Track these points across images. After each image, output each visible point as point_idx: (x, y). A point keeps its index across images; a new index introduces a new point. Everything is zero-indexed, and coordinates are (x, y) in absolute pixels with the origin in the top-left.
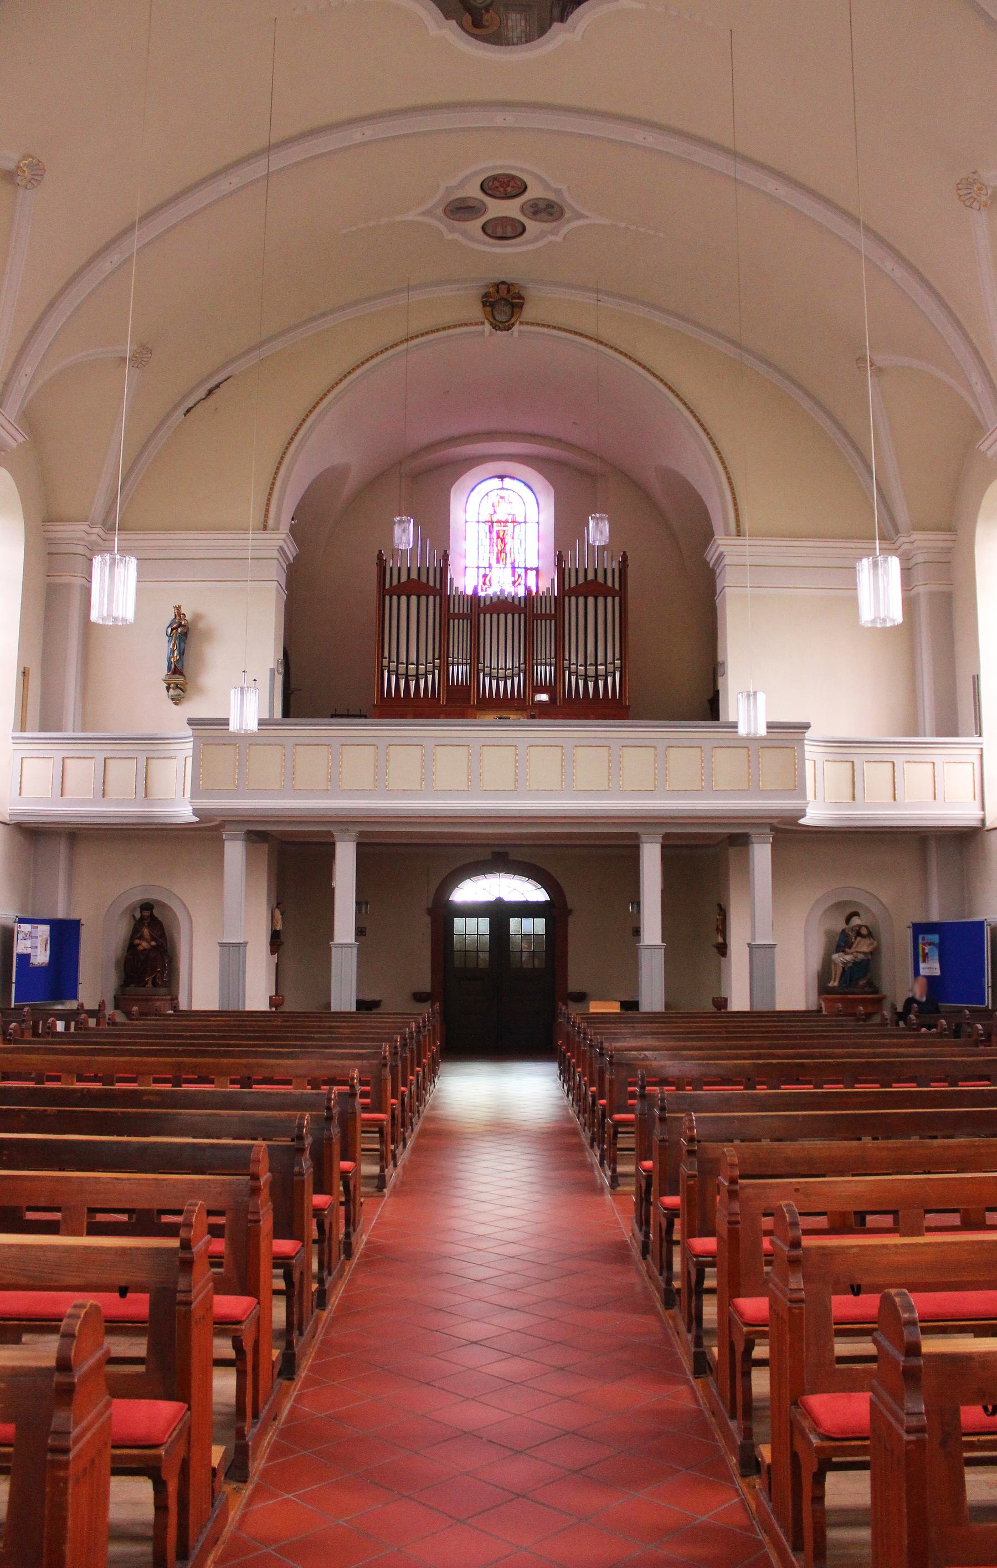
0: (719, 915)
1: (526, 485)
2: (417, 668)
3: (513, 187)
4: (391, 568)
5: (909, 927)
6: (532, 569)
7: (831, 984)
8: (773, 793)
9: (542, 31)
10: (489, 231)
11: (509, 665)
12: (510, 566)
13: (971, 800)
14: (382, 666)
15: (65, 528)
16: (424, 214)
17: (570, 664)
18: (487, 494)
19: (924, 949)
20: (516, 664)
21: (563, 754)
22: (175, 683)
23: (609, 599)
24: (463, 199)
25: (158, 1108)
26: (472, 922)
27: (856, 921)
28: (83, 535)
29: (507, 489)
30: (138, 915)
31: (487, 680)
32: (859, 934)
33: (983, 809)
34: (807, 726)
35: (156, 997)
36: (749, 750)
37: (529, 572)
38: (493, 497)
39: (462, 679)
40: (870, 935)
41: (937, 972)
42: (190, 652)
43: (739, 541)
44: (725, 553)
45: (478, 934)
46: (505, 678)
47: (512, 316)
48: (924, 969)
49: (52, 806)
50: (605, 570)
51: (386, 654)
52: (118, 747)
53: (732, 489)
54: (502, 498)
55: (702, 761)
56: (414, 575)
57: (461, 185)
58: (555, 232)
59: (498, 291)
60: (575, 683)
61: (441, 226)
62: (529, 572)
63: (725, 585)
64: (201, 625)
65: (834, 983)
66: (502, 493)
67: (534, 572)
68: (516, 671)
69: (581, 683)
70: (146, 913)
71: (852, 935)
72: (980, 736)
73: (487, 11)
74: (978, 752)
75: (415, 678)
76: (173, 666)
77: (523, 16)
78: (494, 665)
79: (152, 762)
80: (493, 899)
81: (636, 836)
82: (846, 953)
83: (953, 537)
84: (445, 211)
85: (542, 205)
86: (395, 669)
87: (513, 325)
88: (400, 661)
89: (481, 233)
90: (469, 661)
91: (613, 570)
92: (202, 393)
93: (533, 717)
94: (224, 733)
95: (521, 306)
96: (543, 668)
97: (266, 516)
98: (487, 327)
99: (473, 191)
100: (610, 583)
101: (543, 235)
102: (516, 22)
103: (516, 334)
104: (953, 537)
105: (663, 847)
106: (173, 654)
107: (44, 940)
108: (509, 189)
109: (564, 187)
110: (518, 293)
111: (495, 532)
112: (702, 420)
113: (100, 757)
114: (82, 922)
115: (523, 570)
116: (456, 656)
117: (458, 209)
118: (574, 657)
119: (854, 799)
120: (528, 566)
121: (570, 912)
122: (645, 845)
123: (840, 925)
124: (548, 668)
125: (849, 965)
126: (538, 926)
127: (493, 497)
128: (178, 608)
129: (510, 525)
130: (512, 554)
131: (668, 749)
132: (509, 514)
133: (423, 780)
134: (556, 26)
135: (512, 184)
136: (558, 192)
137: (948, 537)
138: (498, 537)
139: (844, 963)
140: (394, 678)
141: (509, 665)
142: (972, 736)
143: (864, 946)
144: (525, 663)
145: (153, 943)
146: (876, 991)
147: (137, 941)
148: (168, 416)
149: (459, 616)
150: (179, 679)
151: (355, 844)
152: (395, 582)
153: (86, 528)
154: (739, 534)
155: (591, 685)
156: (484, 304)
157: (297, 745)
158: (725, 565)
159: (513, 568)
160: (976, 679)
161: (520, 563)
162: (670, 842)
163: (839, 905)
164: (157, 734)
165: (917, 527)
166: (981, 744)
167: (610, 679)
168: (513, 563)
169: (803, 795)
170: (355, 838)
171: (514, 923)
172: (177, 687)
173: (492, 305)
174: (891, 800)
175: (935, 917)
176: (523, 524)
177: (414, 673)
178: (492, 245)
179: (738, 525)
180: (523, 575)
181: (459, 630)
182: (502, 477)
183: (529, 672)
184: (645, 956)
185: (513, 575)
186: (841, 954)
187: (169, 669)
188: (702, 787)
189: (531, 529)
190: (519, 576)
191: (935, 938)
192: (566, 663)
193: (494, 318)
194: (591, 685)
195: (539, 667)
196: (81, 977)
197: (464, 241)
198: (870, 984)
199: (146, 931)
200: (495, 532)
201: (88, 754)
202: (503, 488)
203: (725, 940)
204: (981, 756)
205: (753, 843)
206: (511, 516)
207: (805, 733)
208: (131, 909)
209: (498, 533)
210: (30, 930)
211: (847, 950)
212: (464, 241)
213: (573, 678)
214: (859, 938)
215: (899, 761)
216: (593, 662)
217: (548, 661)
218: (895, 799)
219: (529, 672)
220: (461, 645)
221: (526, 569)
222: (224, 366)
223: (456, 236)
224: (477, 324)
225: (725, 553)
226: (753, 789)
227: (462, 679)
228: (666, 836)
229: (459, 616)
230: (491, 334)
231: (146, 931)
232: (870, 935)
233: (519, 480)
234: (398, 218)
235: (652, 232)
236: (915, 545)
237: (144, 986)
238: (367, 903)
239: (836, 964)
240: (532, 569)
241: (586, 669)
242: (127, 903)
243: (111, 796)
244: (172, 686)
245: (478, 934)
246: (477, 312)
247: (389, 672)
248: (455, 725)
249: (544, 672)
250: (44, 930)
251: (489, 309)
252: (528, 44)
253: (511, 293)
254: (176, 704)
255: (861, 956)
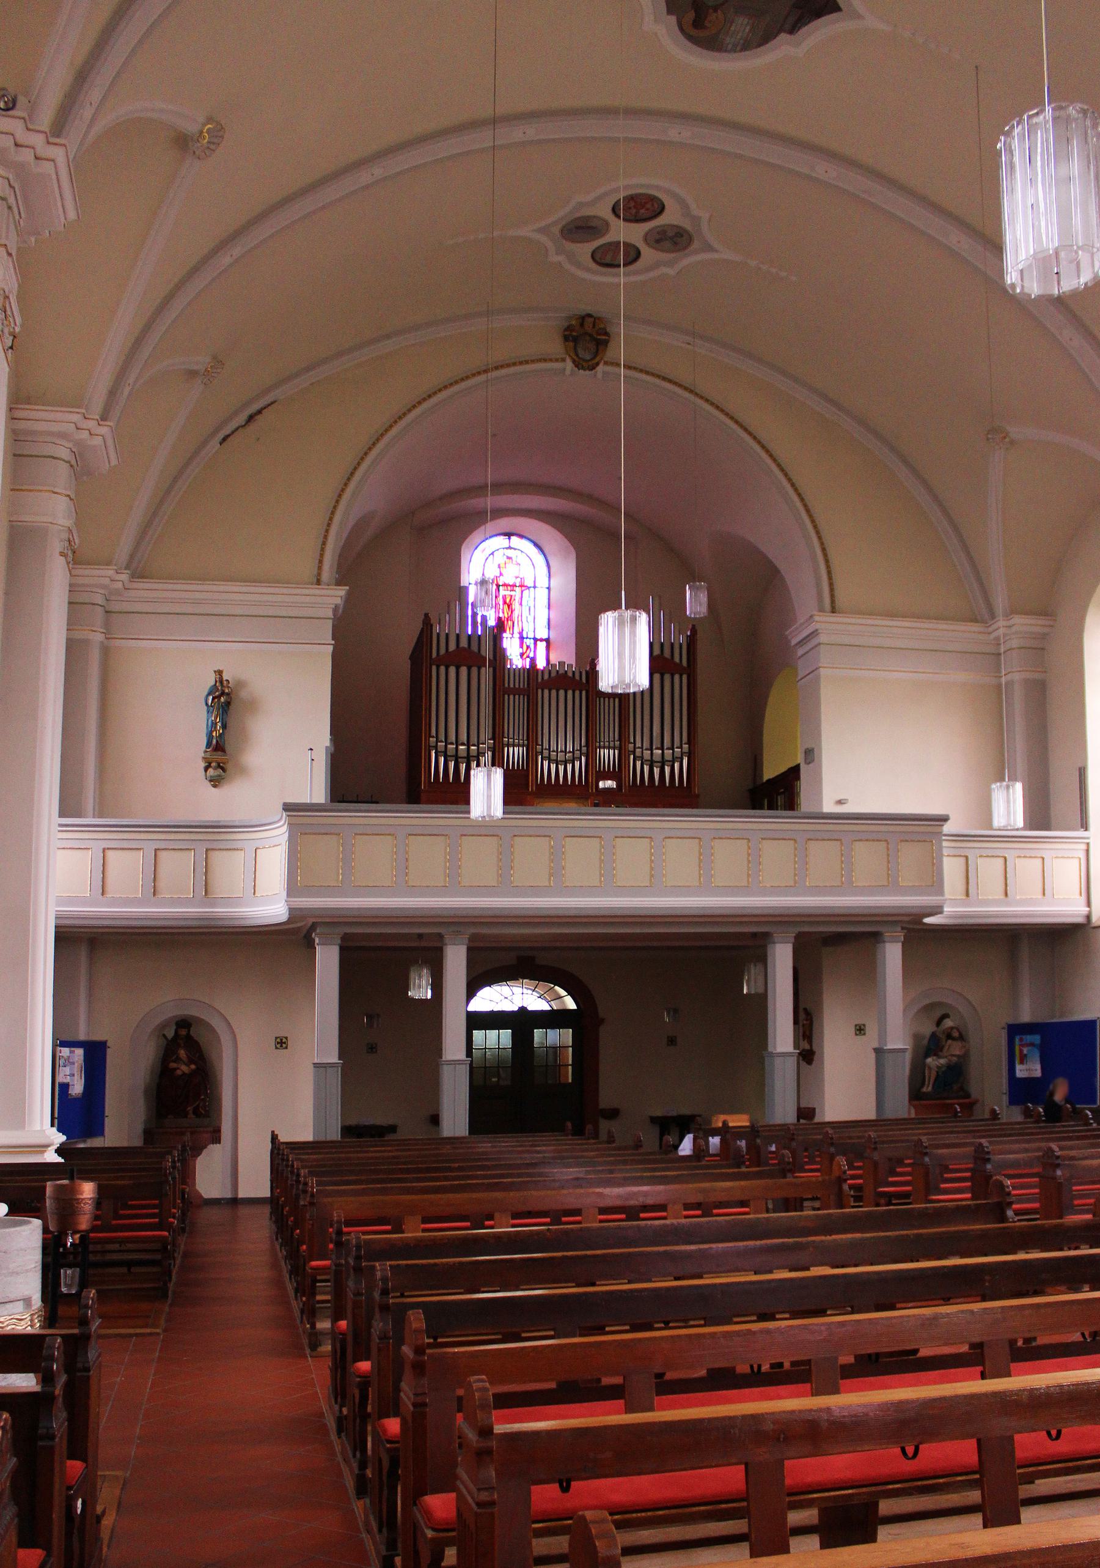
0: (807, 1020)
1: (536, 545)
2: (468, 749)
3: (647, 209)
4: (438, 635)
5: (1003, 1028)
6: (541, 640)
7: (924, 1090)
8: (776, 890)
9: (765, 39)
10: (597, 259)
11: (570, 748)
12: (518, 636)
13: (1078, 897)
14: (503, 744)
15: (87, 572)
16: (541, 230)
17: (635, 748)
18: (493, 553)
19: (1021, 1051)
20: (577, 747)
21: (700, 847)
22: (216, 762)
23: (677, 677)
24: (588, 218)
25: (625, 1247)
26: (492, 1034)
27: (948, 1023)
28: (107, 581)
29: (515, 549)
30: (170, 1033)
31: (546, 763)
32: (949, 1036)
33: (1089, 904)
34: (944, 819)
35: (202, 1129)
36: (842, 844)
37: (538, 642)
38: (499, 558)
39: (513, 763)
40: (961, 1038)
41: (1038, 1073)
42: (231, 723)
43: (833, 618)
44: (819, 631)
45: (499, 1048)
46: (565, 763)
47: (596, 354)
48: (1021, 1071)
49: (91, 906)
50: (672, 645)
51: (433, 733)
52: (172, 837)
53: (827, 561)
54: (509, 558)
55: (842, 855)
56: (464, 643)
57: (593, 203)
58: (670, 264)
59: (582, 325)
60: (639, 769)
61: (550, 245)
62: (538, 642)
63: (820, 665)
64: (244, 694)
65: (928, 1089)
66: (510, 553)
67: (544, 643)
68: (577, 753)
69: (646, 768)
70: (183, 1032)
71: (943, 1037)
72: (1086, 830)
73: (715, 11)
74: (1084, 847)
75: (475, 758)
76: (214, 741)
77: (751, 21)
78: (553, 747)
79: (211, 853)
80: (516, 1009)
81: (440, 936)
82: (939, 1057)
83: (1051, 623)
84: (562, 231)
85: (667, 244)
86: (640, 755)
87: (598, 364)
88: (449, 741)
89: (591, 260)
90: (617, 743)
91: (681, 645)
92: (242, 418)
93: (596, 805)
94: (466, 822)
95: (606, 343)
96: (606, 751)
97: (320, 568)
98: (569, 365)
99: (604, 211)
100: (677, 659)
101: (657, 265)
102: (741, 26)
103: (600, 375)
104: (1051, 623)
105: (469, 950)
106: (216, 727)
107: (80, 1066)
108: (642, 211)
109: (704, 215)
110: (605, 329)
111: (501, 597)
112: (797, 485)
113: (150, 848)
114: (108, 1044)
115: (532, 641)
116: (511, 736)
117: (578, 228)
118: (638, 740)
119: (967, 895)
120: (538, 637)
121: (602, 1021)
122: (449, 946)
123: (928, 1029)
124: (611, 752)
125: (943, 1069)
126: (561, 1037)
127: (499, 558)
128: (219, 673)
129: (518, 590)
130: (520, 623)
131: (854, 843)
132: (517, 577)
133: (551, 875)
134: (783, 36)
135: (649, 206)
136: (696, 220)
137: (1047, 623)
138: (505, 602)
139: (938, 1067)
140: (442, 760)
141: (570, 748)
142: (1078, 830)
143: (955, 1049)
144: (587, 745)
145: (193, 1067)
146: (968, 1096)
147: (173, 1065)
148: (204, 443)
149: (515, 692)
150: (219, 756)
151: (465, 947)
152: (443, 651)
153: (111, 573)
154: (833, 610)
155: (656, 771)
156: (566, 338)
157: (410, 835)
158: (820, 644)
159: (522, 638)
160: (1082, 773)
161: (528, 631)
162: (476, 944)
163: (928, 1008)
164: (219, 821)
165: (1013, 611)
166: (1088, 838)
167: (677, 765)
168: (521, 633)
169: (940, 891)
170: (467, 941)
171: (538, 1033)
172: (219, 766)
173: (575, 340)
174: (1002, 897)
175: (1026, 1017)
176: (532, 589)
177: (659, 759)
178: (604, 274)
179: (833, 601)
180: (532, 646)
181: (515, 706)
182: (509, 535)
183: (590, 756)
184: (446, 1072)
185: (521, 646)
186: (935, 1058)
187: (209, 744)
188: (795, 882)
189: (542, 595)
190: (528, 647)
191: (1036, 1039)
192: (631, 746)
193: (577, 355)
194: (656, 771)
195: (602, 751)
196: (108, 1111)
197: (567, 266)
198: (962, 1089)
199: (182, 1053)
200: (501, 597)
201: (134, 845)
202: (510, 548)
203: (811, 1046)
204: (1087, 851)
205: (774, 943)
206: (519, 580)
207: (943, 825)
208: (164, 1025)
209: (504, 597)
210: (68, 1054)
211: (940, 1053)
212: (567, 266)
213: (638, 764)
214: (950, 1042)
215: (971, 855)
216: (649, 747)
217: (612, 744)
218: (1006, 894)
219: (590, 756)
220: (516, 725)
221: (536, 640)
222: (269, 390)
223: (561, 258)
224: (557, 360)
225: (819, 631)
226: (892, 885)
227: (513, 763)
228: (345, 937)
229: (515, 692)
230: (572, 374)
231: (182, 1053)
232: (961, 1038)
233: (529, 539)
234: (512, 233)
235: (784, 274)
236: (1014, 629)
237: (186, 1117)
238: (378, 1015)
239: (930, 1068)
240: (541, 640)
241: (652, 754)
242: (158, 1021)
243: (165, 894)
244: (213, 764)
245: (499, 1048)
246: (556, 347)
247: (436, 753)
248: (601, 814)
249: (607, 755)
250: (79, 1052)
251: (571, 344)
252: (743, 53)
253: (597, 327)
254: (215, 786)
255: (955, 1059)
